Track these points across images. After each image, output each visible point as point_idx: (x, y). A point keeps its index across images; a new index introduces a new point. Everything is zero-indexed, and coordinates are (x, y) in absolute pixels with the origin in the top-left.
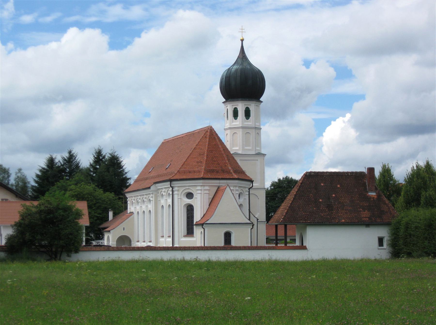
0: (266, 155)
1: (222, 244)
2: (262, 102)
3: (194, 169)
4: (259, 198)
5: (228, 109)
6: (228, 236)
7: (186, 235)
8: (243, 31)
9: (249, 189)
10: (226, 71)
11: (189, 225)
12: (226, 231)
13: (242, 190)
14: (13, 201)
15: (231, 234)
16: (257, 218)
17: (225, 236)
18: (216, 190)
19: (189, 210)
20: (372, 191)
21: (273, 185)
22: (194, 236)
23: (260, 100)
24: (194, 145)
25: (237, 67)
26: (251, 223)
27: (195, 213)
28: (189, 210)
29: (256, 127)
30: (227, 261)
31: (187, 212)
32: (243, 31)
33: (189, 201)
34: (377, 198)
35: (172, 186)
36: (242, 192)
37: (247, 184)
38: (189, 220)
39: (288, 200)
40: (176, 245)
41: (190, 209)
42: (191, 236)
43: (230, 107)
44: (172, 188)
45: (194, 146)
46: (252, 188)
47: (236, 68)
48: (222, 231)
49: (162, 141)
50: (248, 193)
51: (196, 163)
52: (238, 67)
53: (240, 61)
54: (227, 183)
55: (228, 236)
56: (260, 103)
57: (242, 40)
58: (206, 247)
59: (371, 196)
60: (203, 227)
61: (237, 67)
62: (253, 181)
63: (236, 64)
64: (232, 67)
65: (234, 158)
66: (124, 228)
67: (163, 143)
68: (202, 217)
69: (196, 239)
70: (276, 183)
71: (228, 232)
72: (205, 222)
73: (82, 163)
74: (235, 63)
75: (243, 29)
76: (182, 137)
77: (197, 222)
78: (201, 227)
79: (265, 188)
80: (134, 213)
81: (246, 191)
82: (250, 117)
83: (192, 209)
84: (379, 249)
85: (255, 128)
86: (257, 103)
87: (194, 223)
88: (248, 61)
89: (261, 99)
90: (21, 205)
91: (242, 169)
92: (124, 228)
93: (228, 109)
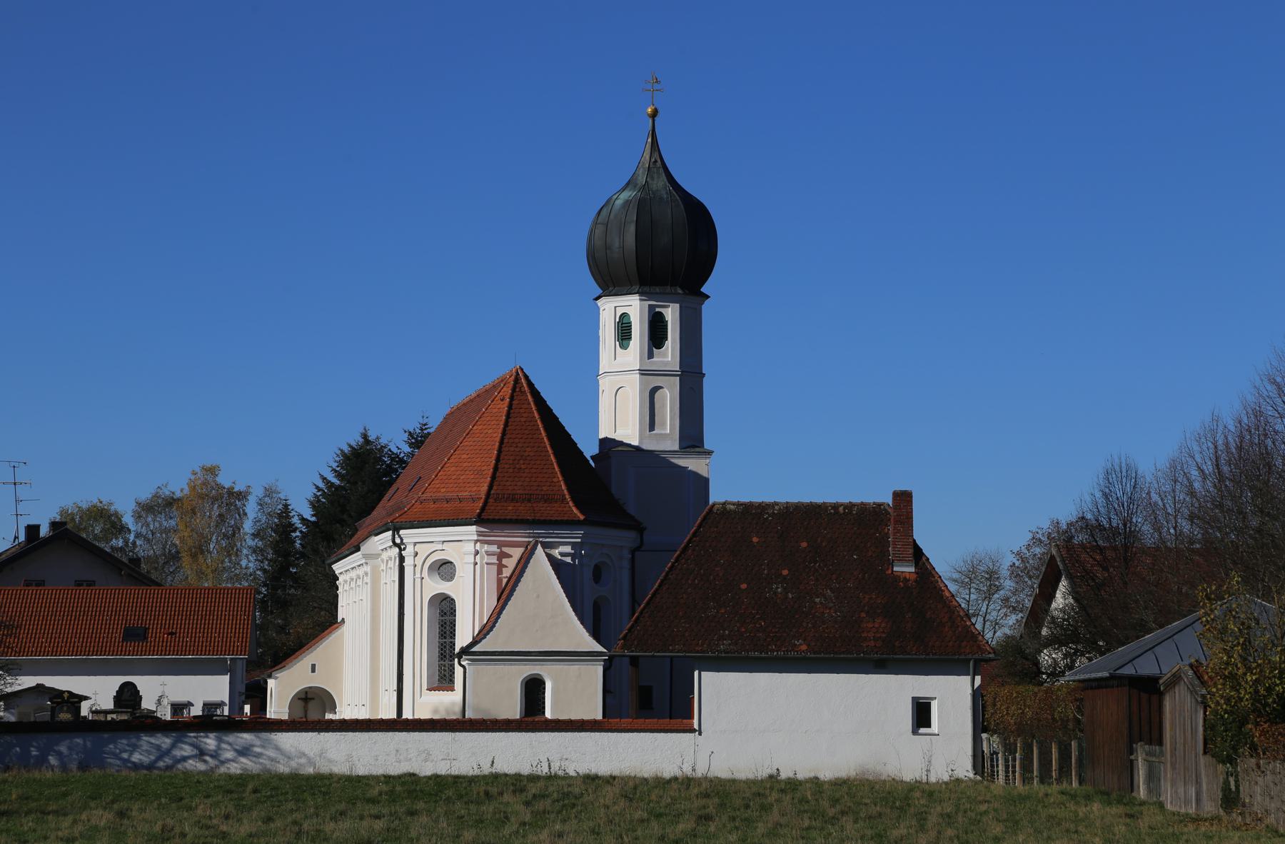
0: (713, 452)
1: (513, 708)
2: (708, 297)
6: (533, 689)
9: (633, 552)
12: (529, 675)
19: (445, 614)
20: (902, 560)
21: (315, 505)
26: (474, 649)
28: (445, 614)
30: (836, 779)
33: (437, 586)
34: (916, 581)
37: (626, 538)
38: (445, 642)
40: (407, 714)
41: (444, 609)
46: (642, 549)
47: (626, 198)
48: (516, 675)
50: (626, 564)
51: (472, 477)
55: (533, 689)
58: (471, 720)
59: (899, 574)
60: (463, 663)
61: (630, 193)
62: (645, 529)
63: (630, 186)
64: (615, 197)
66: (315, 665)
71: (529, 678)
73: (340, 449)
87: (457, 650)
89: (704, 289)
90: (1052, 557)
92: (315, 665)
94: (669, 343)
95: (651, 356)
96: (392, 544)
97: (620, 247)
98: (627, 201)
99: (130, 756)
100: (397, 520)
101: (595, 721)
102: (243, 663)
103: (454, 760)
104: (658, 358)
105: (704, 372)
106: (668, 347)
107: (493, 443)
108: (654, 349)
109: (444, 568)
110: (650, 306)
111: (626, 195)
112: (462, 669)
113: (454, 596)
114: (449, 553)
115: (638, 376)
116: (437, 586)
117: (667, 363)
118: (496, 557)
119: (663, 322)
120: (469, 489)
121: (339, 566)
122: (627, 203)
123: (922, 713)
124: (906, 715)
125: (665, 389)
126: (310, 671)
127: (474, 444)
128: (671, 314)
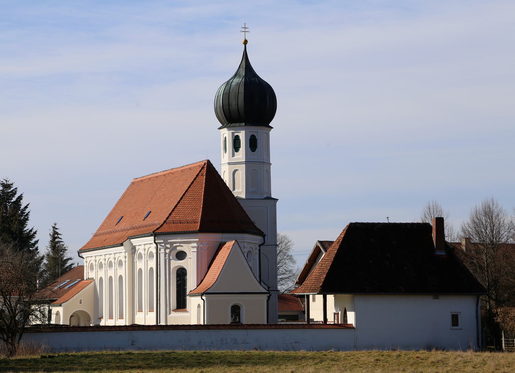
1: (228, 320)
3: (187, 219)
4: (268, 259)
5: (226, 137)
6: (236, 310)
7: (176, 308)
8: (247, 30)
9: (260, 246)
10: (225, 85)
11: (180, 295)
13: (251, 247)
14: (258, 280)
15: (240, 307)
16: (268, 286)
17: (232, 310)
18: (217, 248)
22: (187, 310)
23: (269, 125)
24: (187, 185)
25: (238, 80)
27: (188, 279)
29: (264, 163)
31: (176, 277)
32: (247, 30)
33: (176, 264)
35: (156, 241)
36: (251, 250)
39: (324, 261)
42: (183, 311)
43: (226, 133)
44: (156, 244)
45: (185, 187)
49: (131, 180)
50: (257, 252)
52: (241, 79)
53: (243, 73)
54: (236, 238)
55: (236, 310)
56: (270, 129)
57: (246, 42)
60: (203, 298)
62: (265, 235)
63: (237, 76)
64: (231, 81)
65: (239, 204)
67: (133, 183)
68: (199, 284)
69: (191, 315)
70: (23, 222)
72: (205, 292)
74: (236, 75)
75: (246, 28)
76: (164, 175)
77: (191, 291)
78: (200, 298)
79: (276, 244)
80: (94, 279)
81: (256, 249)
82: (257, 149)
83: (183, 273)
84: (451, 329)
85: (264, 163)
86: (267, 129)
87: (188, 292)
88: (254, 72)
91: (250, 220)
93: (226, 137)
94: (241, 149)
95: (233, 155)
96: (153, 242)
97: (236, 105)
98: (238, 83)
99: (10, 343)
100: (156, 232)
101: (264, 325)
102: (332, 322)
103: (247, 343)
104: (237, 156)
105: (271, 163)
106: (240, 151)
107: (200, 195)
108: (235, 152)
109: (181, 255)
110: (232, 132)
111: (237, 80)
112: (203, 301)
113: (186, 268)
114: (185, 248)
115: (228, 165)
116: (176, 264)
117: (239, 158)
118: (196, 249)
119: (239, 140)
120: (192, 217)
121: (88, 254)
122: (238, 84)
123: (455, 319)
124: (449, 320)
125: (239, 171)
126: (82, 300)
127: (191, 196)
128: (242, 135)
